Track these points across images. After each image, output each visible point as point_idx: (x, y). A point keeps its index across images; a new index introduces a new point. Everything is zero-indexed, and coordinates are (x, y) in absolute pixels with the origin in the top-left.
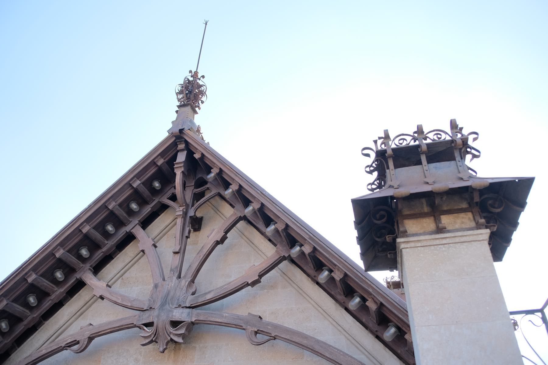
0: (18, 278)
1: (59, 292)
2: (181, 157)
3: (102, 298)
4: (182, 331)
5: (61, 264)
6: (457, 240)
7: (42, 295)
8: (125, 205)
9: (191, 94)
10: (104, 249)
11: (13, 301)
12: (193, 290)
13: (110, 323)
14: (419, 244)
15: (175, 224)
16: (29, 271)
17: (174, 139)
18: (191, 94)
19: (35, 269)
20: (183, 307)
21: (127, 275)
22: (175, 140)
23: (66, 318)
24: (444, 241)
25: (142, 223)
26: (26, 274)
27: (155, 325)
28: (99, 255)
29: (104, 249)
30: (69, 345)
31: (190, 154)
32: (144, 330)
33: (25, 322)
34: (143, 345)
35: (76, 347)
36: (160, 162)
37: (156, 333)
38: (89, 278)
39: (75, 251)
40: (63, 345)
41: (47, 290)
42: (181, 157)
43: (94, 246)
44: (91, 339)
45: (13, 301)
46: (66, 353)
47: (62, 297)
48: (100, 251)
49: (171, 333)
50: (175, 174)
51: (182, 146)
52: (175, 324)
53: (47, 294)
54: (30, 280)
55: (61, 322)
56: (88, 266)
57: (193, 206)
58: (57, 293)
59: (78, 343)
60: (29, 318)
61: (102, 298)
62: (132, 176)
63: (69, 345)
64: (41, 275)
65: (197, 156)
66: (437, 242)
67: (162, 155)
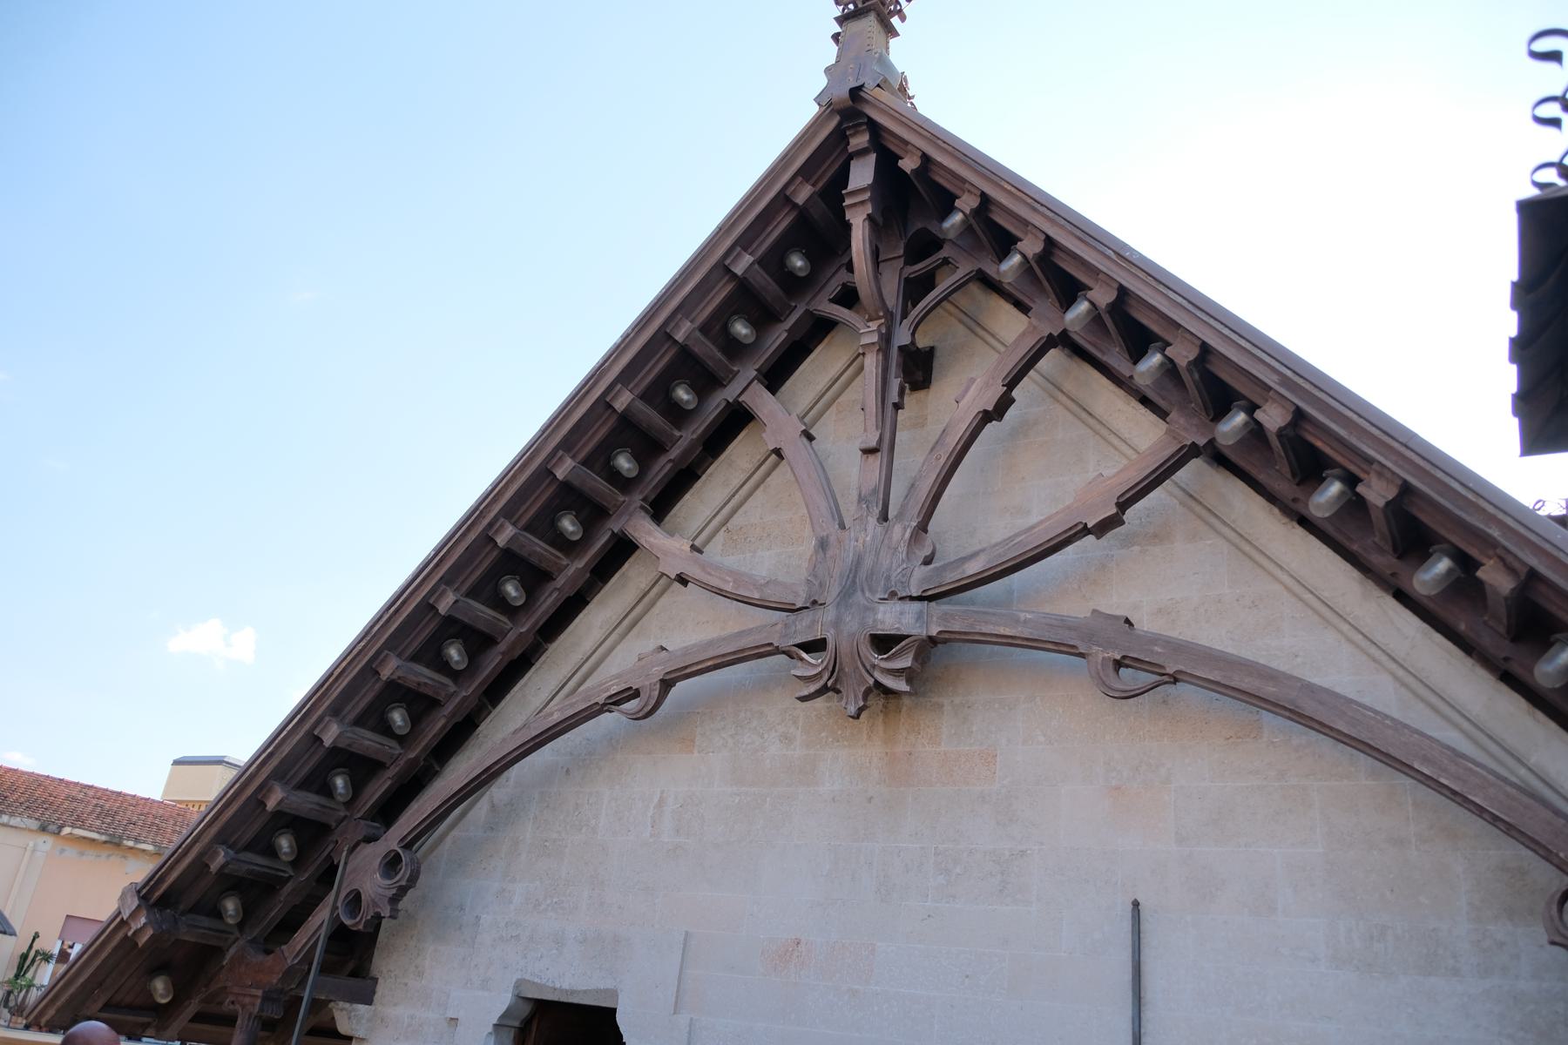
1: (573, 569)
2: (862, 174)
3: (683, 580)
4: (906, 662)
8: (717, 328)
12: (927, 552)
15: (862, 368)
16: (496, 519)
17: (836, 120)
20: (901, 599)
21: (737, 520)
22: (840, 124)
23: (596, 634)
25: (765, 376)
26: (491, 525)
27: (830, 645)
28: (662, 468)
30: (617, 700)
32: (802, 659)
33: (502, 647)
34: (803, 699)
35: (632, 705)
36: (803, 194)
37: (834, 668)
38: (644, 530)
41: (544, 565)
42: (862, 174)
44: (667, 684)
48: (663, 460)
49: (874, 666)
50: (847, 227)
52: (884, 643)
54: (501, 540)
55: (588, 645)
56: (637, 499)
57: (905, 315)
59: (636, 694)
61: (683, 580)
62: (728, 243)
63: (617, 700)
64: (527, 528)
65: (908, 164)
67: (805, 172)
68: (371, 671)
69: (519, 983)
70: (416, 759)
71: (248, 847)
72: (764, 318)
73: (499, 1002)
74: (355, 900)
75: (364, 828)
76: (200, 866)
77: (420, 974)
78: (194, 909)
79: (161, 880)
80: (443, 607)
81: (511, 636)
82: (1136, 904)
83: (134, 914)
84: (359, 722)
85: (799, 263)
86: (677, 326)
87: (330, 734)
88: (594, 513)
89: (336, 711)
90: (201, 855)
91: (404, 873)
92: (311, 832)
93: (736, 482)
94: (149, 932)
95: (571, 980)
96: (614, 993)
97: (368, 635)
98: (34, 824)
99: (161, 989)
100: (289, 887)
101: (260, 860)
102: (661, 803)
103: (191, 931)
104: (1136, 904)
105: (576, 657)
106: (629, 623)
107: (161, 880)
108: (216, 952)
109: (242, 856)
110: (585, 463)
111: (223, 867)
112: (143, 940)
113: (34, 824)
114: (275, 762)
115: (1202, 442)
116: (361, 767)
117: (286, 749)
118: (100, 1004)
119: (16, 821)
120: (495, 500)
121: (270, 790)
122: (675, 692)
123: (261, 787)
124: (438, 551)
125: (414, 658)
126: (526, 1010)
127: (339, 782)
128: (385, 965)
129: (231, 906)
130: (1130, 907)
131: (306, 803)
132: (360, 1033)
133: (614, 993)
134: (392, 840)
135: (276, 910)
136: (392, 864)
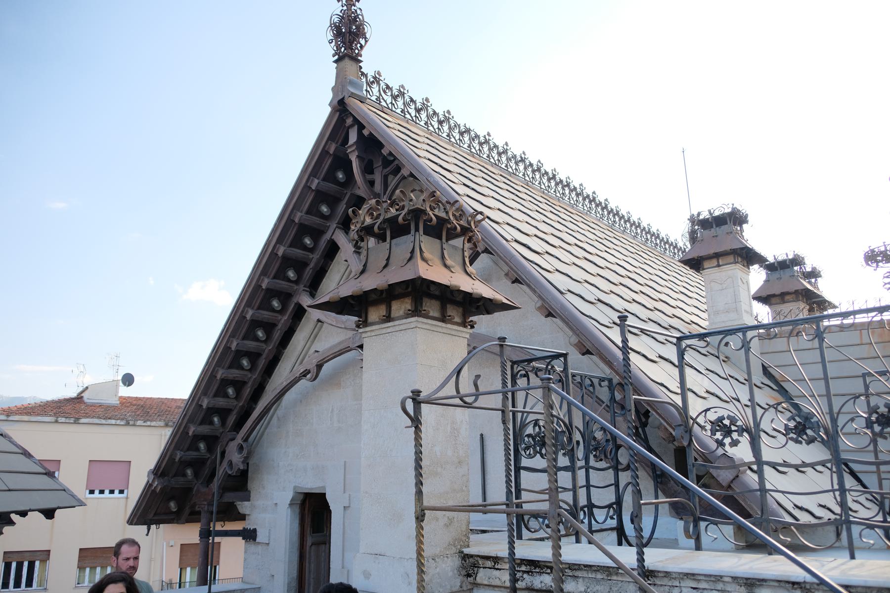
0: (237, 318)
1: (284, 320)
2: (353, 137)
5: (271, 293)
6: (397, 328)
7: (269, 327)
8: (313, 210)
9: (348, 35)
10: (312, 265)
11: (244, 339)
13: (331, 348)
14: (373, 334)
16: (244, 308)
17: (338, 113)
18: (348, 35)
19: (249, 304)
22: (340, 115)
23: (302, 343)
24: (389, 330)
25: (342, 224)
26: (243, 311)
28: (308, 272)
29: (312, 265)
30: (305, 374)
31: (361, 127)
33: (264, 356)
35: (309, 376)
36: (332, 149)
39: (280, 274)
40: (298, 375)
41: (271, 321)
42: (353, 137)
43: (300, 266)
44: (319, 367)
45: (244, 339)
46: (303, 382)
47: (289, 325)
48: (308, 269)
50: (351, 162)
51: (349, 121)
53: (274, 325)
54: (248, 317)
55: (300, 348)
56: (302, 287)
57: (385, 194)
58: (282, 321)
59: (309, 372)
60: (266, 351)
62: (306, 177)
63: (305, 374)
64: (259, 308)
66: (384, 331)
67: (331, 138)
68: (213, 376)
69: (295, 487)
70: (243, 406)
71: (188, 450)
72: (333, 201)
73: (289, 495)
74: (230, 464)
75: (230, 435)
76: (172, 460)
77: (264, 488)
78: (175, 475)
79: (160, 467)
80: (234, 346)
81: (282, 321)
82: (482, 435)
83: (153, 481)
84: (215, 395)
85: (341, 176)
86: (295, 216)
87: (205, 403)
88: (285, 297)
89: (205, 393)
90: (171, 455)
91: (245, 452)
92: (212, 441)
93: (343, 270)
94: (159, 487)
95: (311, 485)
96: (324, 488)
97: (208, 363)
98: (162, 423)
99: (173, 505)
100: (209, 461)
101: (195, 453)
102: (332, 410)
103: (178, 482)
104: (482, 435)
105: (297, 353)
106: (314, 336)
107: (160, 467)
108: (190, 489)
109: (187, 453)
110: (275, 278)
111: (181, 458)
112: (158, 490)
113: (162, 423)
114: (187, 417)
115: (478, 249)
116: (224, 413)
117: (190, 412)
118: (152, 515)
119: (153, 424)
120: (242, 301)
121: (189, 428)
122: (326, 367)
123: (185, 427)
124: (225, 326)
125: (230, 367)
126: (302, 497)
127: (216, 419)
128: (252, 485)
129: (189, 472)
130: (479, 436)
131: (205, 429)
132: (247, 513)
133: (324, 488)
134: (239, 439)
135: (206, 471)
136: (241, 448)
